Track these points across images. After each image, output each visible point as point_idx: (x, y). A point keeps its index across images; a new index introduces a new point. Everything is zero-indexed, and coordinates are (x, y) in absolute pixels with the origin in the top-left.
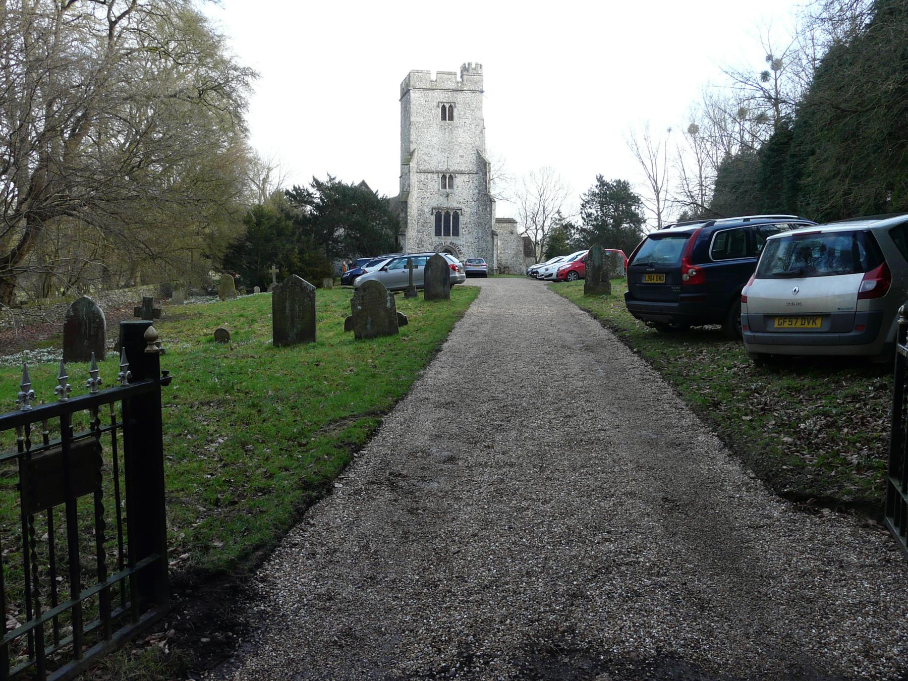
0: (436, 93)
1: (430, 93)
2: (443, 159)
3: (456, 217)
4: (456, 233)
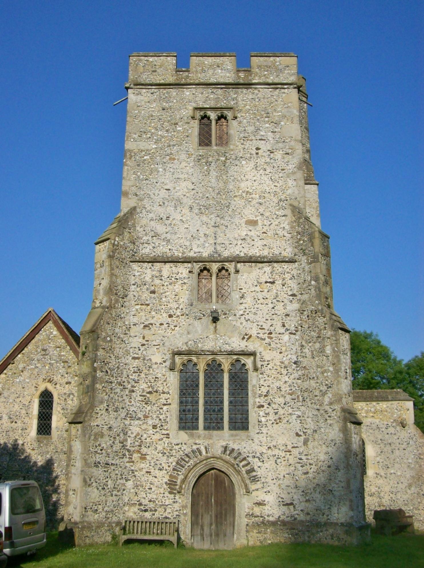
0: (187, 93)
1: (173, 92)
2: (204, 230)
3: (240, 381)
4: (241, 423)
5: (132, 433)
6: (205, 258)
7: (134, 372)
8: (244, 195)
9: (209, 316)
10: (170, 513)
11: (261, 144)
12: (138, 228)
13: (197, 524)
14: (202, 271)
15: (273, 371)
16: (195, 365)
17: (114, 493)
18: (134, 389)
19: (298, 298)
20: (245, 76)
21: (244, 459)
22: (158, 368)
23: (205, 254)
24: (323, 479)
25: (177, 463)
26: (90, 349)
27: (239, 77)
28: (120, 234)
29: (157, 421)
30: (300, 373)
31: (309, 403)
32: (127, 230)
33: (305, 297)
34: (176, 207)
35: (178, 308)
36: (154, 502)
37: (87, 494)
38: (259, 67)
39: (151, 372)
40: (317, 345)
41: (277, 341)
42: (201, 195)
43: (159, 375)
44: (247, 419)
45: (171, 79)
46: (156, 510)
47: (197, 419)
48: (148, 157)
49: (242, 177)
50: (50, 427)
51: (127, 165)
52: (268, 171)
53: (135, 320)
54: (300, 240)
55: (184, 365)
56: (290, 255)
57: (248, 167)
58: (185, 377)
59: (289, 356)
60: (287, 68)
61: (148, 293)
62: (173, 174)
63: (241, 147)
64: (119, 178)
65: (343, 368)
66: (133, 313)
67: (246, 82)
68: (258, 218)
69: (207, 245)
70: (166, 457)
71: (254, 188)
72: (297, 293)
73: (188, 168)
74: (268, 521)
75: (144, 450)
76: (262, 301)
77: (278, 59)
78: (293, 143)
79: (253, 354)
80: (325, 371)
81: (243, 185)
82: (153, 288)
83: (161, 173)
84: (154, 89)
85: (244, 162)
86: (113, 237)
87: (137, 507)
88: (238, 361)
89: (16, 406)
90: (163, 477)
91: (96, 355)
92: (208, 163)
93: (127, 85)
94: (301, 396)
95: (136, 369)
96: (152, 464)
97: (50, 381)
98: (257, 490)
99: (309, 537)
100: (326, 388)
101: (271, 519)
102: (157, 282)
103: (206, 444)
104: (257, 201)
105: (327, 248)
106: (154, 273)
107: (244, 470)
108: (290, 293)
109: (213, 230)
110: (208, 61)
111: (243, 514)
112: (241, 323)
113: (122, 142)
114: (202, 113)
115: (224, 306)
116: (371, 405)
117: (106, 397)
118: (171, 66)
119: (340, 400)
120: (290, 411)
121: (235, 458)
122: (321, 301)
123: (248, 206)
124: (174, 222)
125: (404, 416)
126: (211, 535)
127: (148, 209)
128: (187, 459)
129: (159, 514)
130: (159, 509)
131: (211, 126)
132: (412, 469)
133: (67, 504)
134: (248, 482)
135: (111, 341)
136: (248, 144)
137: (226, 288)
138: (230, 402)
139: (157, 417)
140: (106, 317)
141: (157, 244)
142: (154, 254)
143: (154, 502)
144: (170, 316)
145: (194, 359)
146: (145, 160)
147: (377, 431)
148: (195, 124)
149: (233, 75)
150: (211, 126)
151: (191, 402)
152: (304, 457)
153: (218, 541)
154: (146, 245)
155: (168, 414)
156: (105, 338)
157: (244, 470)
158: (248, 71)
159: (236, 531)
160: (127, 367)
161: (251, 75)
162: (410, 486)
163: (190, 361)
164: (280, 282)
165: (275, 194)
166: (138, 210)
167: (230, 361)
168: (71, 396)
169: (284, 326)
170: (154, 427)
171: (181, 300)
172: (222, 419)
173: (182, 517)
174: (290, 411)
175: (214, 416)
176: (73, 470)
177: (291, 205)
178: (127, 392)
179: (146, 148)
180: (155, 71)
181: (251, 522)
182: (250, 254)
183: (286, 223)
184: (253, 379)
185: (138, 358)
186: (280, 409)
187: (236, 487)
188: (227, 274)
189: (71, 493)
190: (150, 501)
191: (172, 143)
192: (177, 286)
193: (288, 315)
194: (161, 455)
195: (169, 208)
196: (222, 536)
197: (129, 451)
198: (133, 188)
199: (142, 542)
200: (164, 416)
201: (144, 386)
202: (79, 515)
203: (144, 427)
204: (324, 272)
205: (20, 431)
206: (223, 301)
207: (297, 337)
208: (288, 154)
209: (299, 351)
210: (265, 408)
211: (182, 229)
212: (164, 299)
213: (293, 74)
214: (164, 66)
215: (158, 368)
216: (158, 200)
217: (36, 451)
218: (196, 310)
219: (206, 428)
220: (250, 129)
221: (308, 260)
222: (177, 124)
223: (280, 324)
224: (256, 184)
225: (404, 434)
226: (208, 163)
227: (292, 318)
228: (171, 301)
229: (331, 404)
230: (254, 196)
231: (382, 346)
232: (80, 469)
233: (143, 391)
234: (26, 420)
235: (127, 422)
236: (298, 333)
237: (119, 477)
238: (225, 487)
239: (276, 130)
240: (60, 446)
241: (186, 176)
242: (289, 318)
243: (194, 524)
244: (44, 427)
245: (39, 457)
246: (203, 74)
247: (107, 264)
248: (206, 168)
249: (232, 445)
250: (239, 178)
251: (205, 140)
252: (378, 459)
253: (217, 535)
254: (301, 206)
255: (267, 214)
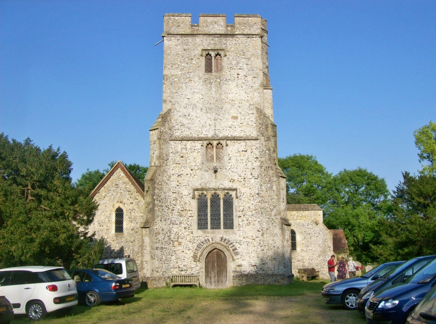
0: (198, 39)
1: (190, 39)
2: (209, 122)
3: (229, 203)
4: (229, 225)
5: (174, 232)
6: (209, 138)
7: (174, 200)
8: (230, 101)
9: (212, 169)
10: (194, 272)
11: (240, 72)
12: (172, 121)
13: (208, 277)
14: (208, 145)
15: (246, 198)
16: (205, 195)
17: (166, 262)
18: (174, 209)
19: (259, 159)
20: (231, 29)
21: (232, 243)
22: (186, 197)
23: (210, 136)
24: (271, 253)
25: (197, 246)
26: (151, 189)
27: (228, 30)
28: (163, 125)
29: (186, 225)
30: (260, 199)
31: (264, 215)
32: (167, 123)
33: (263, 159)
34: (193, 109)
35: (196, 165)
36: (186, 266)
37: (153, 263)
38: (239, 24)
39: (183, 200)
40: (269, 185)
41: (248, 183)
42: (207, 102)
43: (187, 202)
44: (233, 223)
45: (189, 31)
46: (187, 270)
47: (207, 224)
48: (177, 79)
49: (229, 91)
50: (123, 228)
51: (165, 84)
52: (244, 87)
53: (173, 172)
54: (261, 128)
55: (199, 196)
56: (255, 136)
57: (232, 85)
58: (200, 202)
59: (255, 190)
60: (255, 24)
61: (179, 157)
62: (191, 90)
63: (229, 73)
64: (161, 92)
65: (282, 197)
66: (172, 169)
67: (232, 34)
68: (238, 115)
69: (210, 130)
70: (191, 243)
71: (236, 98)
72: (259, 157)
73: (199, 86)
74: (244, 274)
75: (180, 240)
76: (240, 161)
77: (250, 19)
78: (258, 71)
79: (235, 190)
80: (273, 199)
81: (230, 96)
82: (182, 155)
83: (184, 89)
84: (179, 37)
85: (230, 83)
86: (160, 128)
87: (178, 269)
88: (228, 193)
89: (102, 217)
90: (190, 254)
91: (154, 192)
92: (211, 83)
93: (163, 35)
94: (261, 211)
95: (174, 198)
96: (185, 247)
97: (121, 202)
98: (238, 259)
99: (264, 281)
100: (273, 207)
101: (245, 273)
102: (184, 151)
103: (212, 236)
104: (238, 105)
105: (275, 132)
106: (182, 146)
107: (231, 249)
108: (255, 157)
109: (213, 122)
110: (210, 19)
111: (231, 271)
112: (229, 173)
113: (162, 71)
114: (207, 53)
115: (220, 164)
116: (300, 213)
117: (160, 214)
118: (188, 23)
119: (280, 214)
120: (255, 219)
121: (227, 243)
122: (271, 161)
123: (233, 108)
124: (192, 117)
125: (317, 219)
126: (215, 282)
127: (178, 110)
128: (202, 244)
129: (189, 272)
130: (189, 270)
131: (211, 61)
132: (321, 247)
133: (142, 268)
134: (233, 255)
135: (161, 184)
136: (232, 71)
137: (221, 154)
138: (224, 215)
139: (187, 223)
140: (158, 172)
141: (183, 130)
142: (182, 136)
143: (186, 266)
144: (192, 170)
145: (205, 192)
146: (175, 81)
147: (302, 227)
148: (203, 59)
149: (224, 29)
150: (211, 61)
151: (204, 215)
152: (262, 242)
153: (218, 285)
154: (177, 131)
155: (192, 222)
156: (158, 183)
157: (231, 249)
158: (233, 26)
159: (227, 280)
160: (170, 197)
161: (234, 29)
162: (319, 256)
163: (203, 193)
164: (250, 151)
165: (248, 101)
166: (172, 111)
167: (223, 193)
168: (134, 211)
169: (252, 174)
170: (185, 228)
171: (197, 161)
172: (220, 223)
173: (201, 273)
174: (255, 219)
175: (216, 222)
176: (145, 252)
177: (256, 107)
178: (170, 211)
179: (175, 74)
180: (179, 26)
181: (235, 275)
182: (234, 135)
183: (253, 118)
184: (236, 203)
185: (175, 193)
186: (250, 218)
187: (228, 257)
188: (221, 146)
189: (144, 263)
190: (184, 266)
191: (190, 71)
192: (195, 153)
193: (254, 169)
194: (189, 242)
195: (189, 109)
196: (220, 282)
197: (172, 241)
198: (169, 98)
199: (181, 286)
200: (190, 222)
201: (179, 207)
202: (149, 274)
203: (180, 228)
204: (273, 145)
205: (105, 231)
206: (219, 161)
207: (259, 181)
208: (255, 77)
209: (260, 188)
210: (242, 217)
211: (197, 122)
212: (188, 161)
213: (259, 29)
214: (183, 22)
215: (186, 197)
216: (183, 105)
217: (115, 242)
218: (205, 166)
219: (212, 228)
220: (234, 62)
221: (265, 139)
222: (192, 59)
223: (250, 174)
224: (237, 95)
225: (317, 228)
226: (211, 83)
227: (256, 171)
228: (192, 162)
229: (275, 215)
230: (236, 102)
231: (318, 165)
232: (149, 251)
233: (179, 210)
234: (109, 225)
235: (171, 226)
236: (259, 178)
237: (168, 254)
238: (222, 258)
239: (249, 63)
240: (129, 238)
241: (198, 91)
242: (254, 170)
243: (207, 276)
244: (119, 228)
245: (117, 245)
246: (207, 28)
247: (157, 142)
248: (209, 86)
249: (225, 237)
250: (228, 92)
251: (209, 69)
252: (303, 242)
253: (218, 282)
254: (262, 108)
255: (243, 113)
